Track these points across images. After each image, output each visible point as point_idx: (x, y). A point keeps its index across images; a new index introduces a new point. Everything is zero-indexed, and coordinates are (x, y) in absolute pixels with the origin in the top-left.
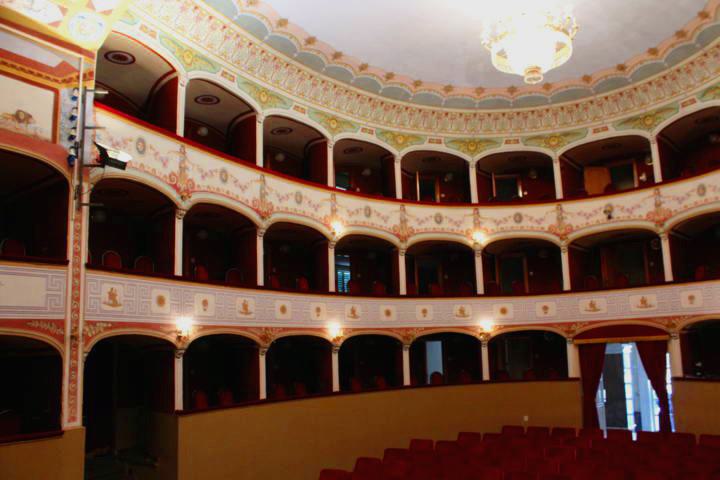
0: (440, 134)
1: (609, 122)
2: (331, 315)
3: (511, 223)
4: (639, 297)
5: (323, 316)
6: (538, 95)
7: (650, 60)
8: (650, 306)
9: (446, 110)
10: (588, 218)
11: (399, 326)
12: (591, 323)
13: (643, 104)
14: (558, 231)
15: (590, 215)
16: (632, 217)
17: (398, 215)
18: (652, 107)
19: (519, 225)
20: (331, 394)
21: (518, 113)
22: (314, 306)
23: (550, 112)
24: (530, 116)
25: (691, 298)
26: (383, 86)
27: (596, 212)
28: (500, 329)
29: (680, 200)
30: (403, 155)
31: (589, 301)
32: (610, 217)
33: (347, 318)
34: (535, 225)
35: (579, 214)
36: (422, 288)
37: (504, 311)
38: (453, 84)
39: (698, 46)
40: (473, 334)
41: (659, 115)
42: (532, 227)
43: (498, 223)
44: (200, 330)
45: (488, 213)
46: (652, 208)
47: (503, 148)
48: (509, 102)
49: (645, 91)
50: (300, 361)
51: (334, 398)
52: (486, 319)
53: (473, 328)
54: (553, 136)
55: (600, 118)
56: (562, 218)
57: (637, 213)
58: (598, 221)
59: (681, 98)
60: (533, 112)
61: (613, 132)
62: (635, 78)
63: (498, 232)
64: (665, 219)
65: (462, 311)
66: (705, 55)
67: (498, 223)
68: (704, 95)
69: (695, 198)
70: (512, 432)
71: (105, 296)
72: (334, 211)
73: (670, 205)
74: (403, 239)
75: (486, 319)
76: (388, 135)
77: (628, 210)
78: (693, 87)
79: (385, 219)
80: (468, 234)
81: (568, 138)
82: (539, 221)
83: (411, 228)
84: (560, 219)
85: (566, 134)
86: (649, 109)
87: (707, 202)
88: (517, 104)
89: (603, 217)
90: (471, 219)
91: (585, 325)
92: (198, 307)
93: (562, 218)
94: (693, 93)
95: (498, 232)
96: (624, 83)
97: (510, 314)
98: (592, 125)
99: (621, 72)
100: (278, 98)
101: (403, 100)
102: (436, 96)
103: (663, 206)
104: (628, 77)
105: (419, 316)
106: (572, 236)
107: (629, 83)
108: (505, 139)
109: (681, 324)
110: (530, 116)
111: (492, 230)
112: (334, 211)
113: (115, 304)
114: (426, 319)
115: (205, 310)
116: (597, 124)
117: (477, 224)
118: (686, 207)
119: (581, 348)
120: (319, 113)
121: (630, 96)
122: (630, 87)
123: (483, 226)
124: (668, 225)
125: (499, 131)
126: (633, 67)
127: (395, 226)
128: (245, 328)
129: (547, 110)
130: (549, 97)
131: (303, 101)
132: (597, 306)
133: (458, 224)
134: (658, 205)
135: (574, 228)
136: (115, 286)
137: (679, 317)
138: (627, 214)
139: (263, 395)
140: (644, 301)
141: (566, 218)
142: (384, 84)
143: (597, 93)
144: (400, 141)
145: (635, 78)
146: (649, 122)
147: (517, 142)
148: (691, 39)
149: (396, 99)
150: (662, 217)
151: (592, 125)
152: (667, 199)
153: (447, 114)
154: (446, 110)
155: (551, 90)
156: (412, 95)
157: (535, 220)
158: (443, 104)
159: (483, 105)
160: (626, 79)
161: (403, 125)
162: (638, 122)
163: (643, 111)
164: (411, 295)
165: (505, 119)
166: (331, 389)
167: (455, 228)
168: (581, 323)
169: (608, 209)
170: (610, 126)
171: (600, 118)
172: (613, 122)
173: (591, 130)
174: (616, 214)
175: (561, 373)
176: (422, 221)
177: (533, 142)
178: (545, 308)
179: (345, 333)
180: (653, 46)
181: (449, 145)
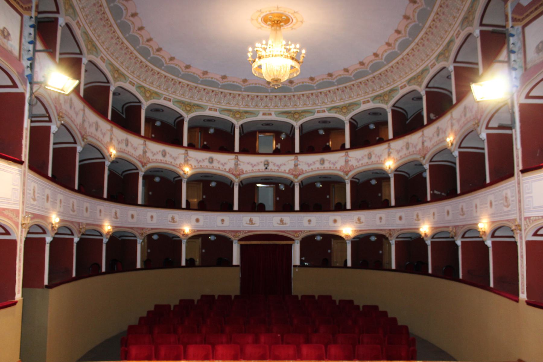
0: (171, 95)
1: (273, 110)
2: (344, 223)
3: (206, 163)
4: (279, 218)
5: (339, 223)
6: (238, 84)
7: (309, 83)
8: (285, 224)
9: (180, 80)
10: (253, 167)
11: (136, 226)
12: (249, 231)
13: (295, 105)
14: (234, 172)
15: (255, 165)
16: (280, 171)
17: (233, 162)
18: (300, 108)
19: (211, 165)
20: (180, 266)
21: (222, 93)
22: (99, 207)
23: (241, 96)
24: (228, 96)
25: (310, 221)
26: (152, 55)
27: (258, 164)
28: (194, 232)
29: (309, 165)
30: (148, 105)
31: (249, 218)
32: (266, 168)
33: (356, 224)
34: (221, 167)
35: (248, 163)
36: (152, 202)
37: (197, 220)
38: (191, 65)
39: (336, 83)
40: (179, 234)
41: (304, 114)
42: (219, 168)
43: (199, 162)
44: (432, 230)
45: (192, 153)
46: (292, 167)
47: (207, 113)
48: (219, 85)
49: (299, 98)
50: (164, 248)
51: (183, 269)
52: (186, 224)
53: (179, 231)
54: (238, 112)
55: (268, 107)
56: (238, 165)
57: (282, 168)
58: (259, 170)
59: (317, 108)
60: (230, 94)
61: (273, 117)
62: (297, 90)
63: (198, 168)
64: (300, 175)
65: (173, 219)
66: (338, 89)
67: (199, 162)
68: (85, 32)
69: (318, 165)
70: (207, 300)
71: (170, 218)
72: (111, 139)
73: (303, 167)
74: (144, 165)
75: (186, 224)
76: (142, 89)
77: (278, 166)
78: (326, 104)
79: (135, 149)
80: (180, 166)
81: (247, 115)
82: (223, 165)
83: (148, 157)
84: (236, 165)
85: (246, 112)
86: (298, 109)
87: (324, 169)
88: (224, 87)
89: (262, 167)
90: (183, 156)
91: (246, 233)
92: (194, 223)
93: (238, 165)
94: (324, 107)
95: (198, 168)
96: (289, 90)
97: (201, 223)
98: (262, 110)
99: (290, 84)
100: (95, 48)
101: (158, 67)
102: (178, 70)
103: (299, 166)
104: (292, 88)
105: (219, 223)
106: (242, 177)
107: (291, 92)
108: (209, 107)
109: (303, 235)
110: (228, 96)
111: (195, 166)
112: (111, 139)
113: (252, 224)
114: (223, 225)
115: (381, 222)
116: (266, 110)
117: (186, 161)
118: (312, 169)
119: (242, 247)
120: (112, 64)
121: (290, 99)
122: (292, 94)
123: (190, 163)
124: (300, 178)
125: (207, 102)
126: (297, 84)
127: (140, 155)
128: (381, 230)
129: (239, 95)
130: (243, 87)
131: (268, 110)
132: (253, 222)
133: (175, 159)
134: (296, 165)
135: (244, 172)
136: (174, 215)
137: (301, 231)
138: (277, 168)
139: (104, 270)
140: (282, 221)
141: (240, 165)
142: (154, 54)
143: (272, 92)
144: (148, 95)
145: (297, 90)
146: (296, 116)
147: (216, 110)
148: (334, 79)
149: (155, 66)
150: (297, 173)
151: (262, 110)
152: (301, 163)
153: (180, 83)
154: (180, 80)
155: (246, 84)
156: (165, 65)
157: (222, 164)
158: (180, 75)
159: (224, 87)
160: (291, 89)
161: (152, 84)
162: (290, 115)
163: (294, 109)
164: (241, 210)
165: (213, 94)
166: (136, 266)
167: (173, 161)
168: (243, 231)
169: (266, 163)
170: (273, 113)
171: (268, 107)
172: (275, 111)
173: (261, 113)
174: (271, 167)
175: (228, 262)
176: (155, 154)
177: (226, 113)
178: (310, 221)
179: (113, 229)
180: (313, 76)
181: (176, 104)
